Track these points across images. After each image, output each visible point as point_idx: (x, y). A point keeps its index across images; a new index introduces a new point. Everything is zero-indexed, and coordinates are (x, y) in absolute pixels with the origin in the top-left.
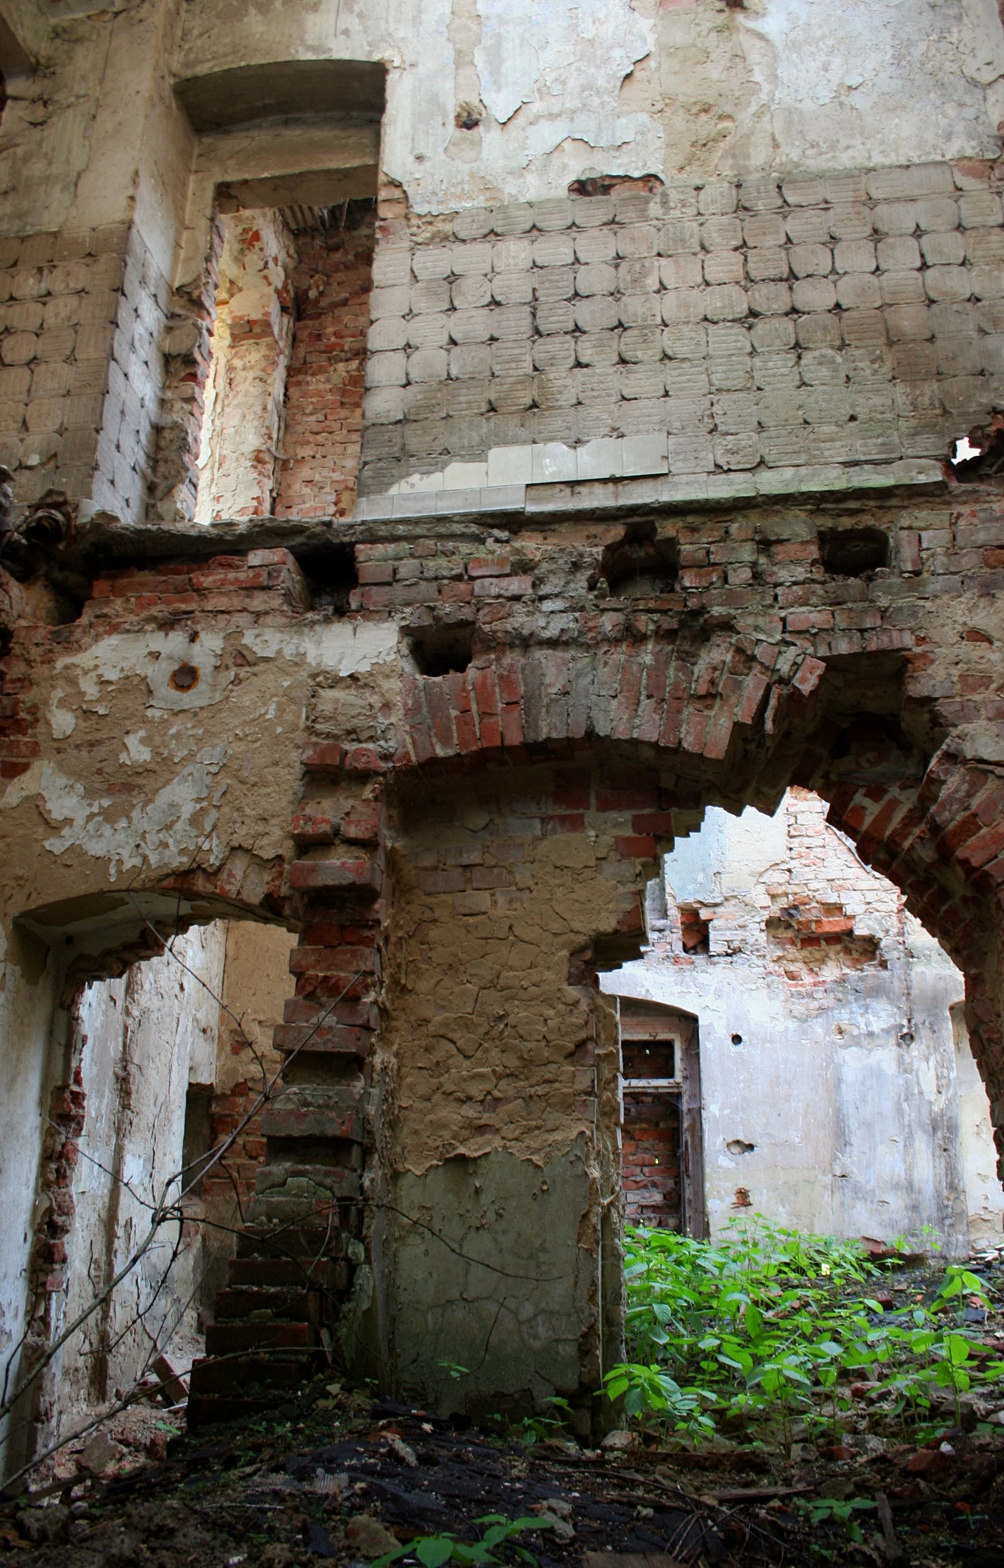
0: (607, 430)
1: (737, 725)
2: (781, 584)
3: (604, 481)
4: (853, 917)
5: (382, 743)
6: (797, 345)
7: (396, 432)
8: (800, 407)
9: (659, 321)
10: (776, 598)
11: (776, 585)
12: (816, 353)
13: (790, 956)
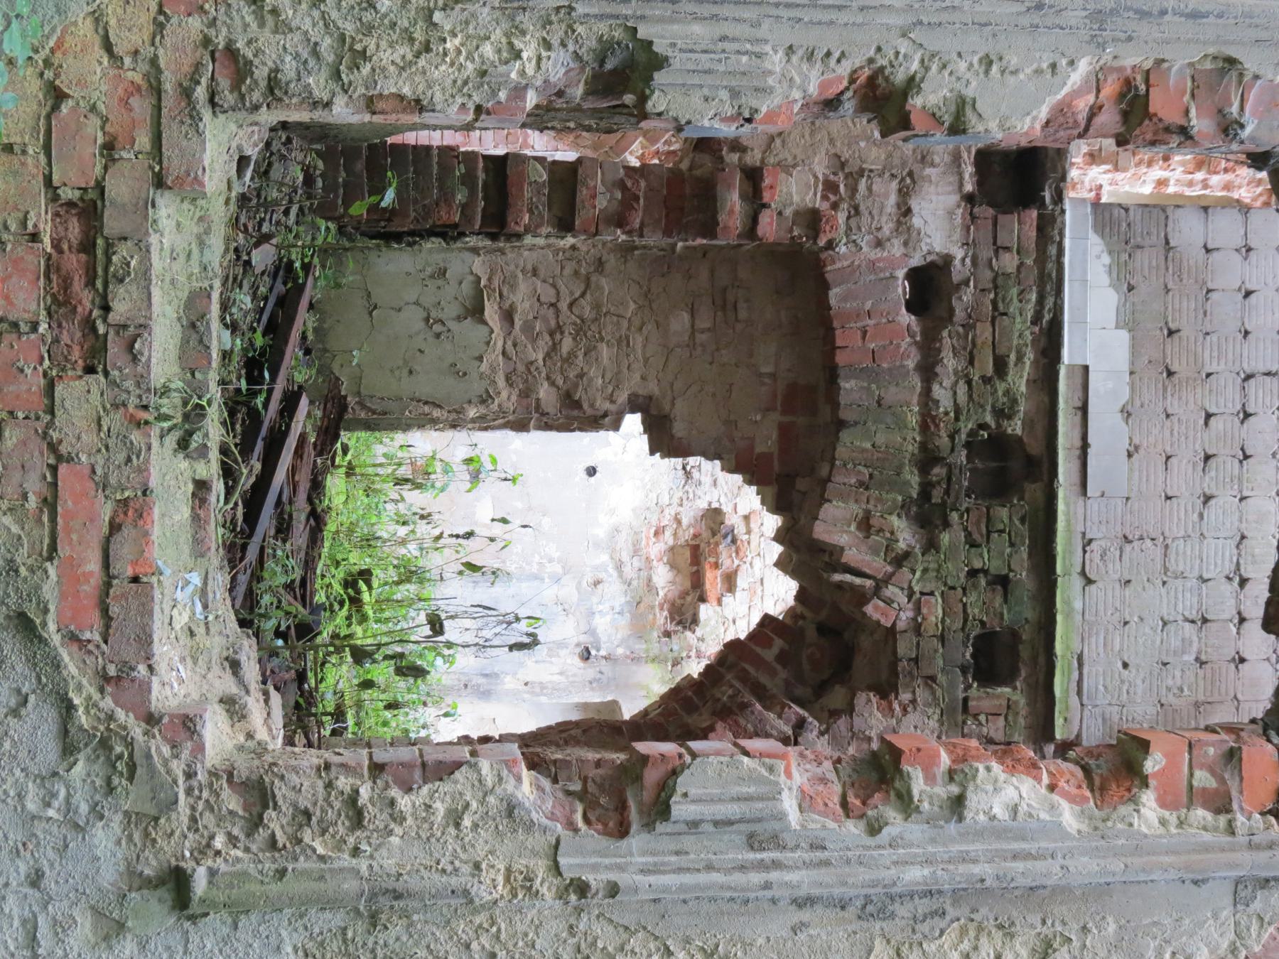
0: (1136, 441)
1: (842, 549)
2: (965, 594)
4: (719, 602)
5: (844, 240)
6: (1205, 621)
7: (1156, 239)
8: (1141, 619)
9: (1245, 493)
10: (953, 588)
11: (964, 589)
12: (1195, 639)
13: (680, 532)
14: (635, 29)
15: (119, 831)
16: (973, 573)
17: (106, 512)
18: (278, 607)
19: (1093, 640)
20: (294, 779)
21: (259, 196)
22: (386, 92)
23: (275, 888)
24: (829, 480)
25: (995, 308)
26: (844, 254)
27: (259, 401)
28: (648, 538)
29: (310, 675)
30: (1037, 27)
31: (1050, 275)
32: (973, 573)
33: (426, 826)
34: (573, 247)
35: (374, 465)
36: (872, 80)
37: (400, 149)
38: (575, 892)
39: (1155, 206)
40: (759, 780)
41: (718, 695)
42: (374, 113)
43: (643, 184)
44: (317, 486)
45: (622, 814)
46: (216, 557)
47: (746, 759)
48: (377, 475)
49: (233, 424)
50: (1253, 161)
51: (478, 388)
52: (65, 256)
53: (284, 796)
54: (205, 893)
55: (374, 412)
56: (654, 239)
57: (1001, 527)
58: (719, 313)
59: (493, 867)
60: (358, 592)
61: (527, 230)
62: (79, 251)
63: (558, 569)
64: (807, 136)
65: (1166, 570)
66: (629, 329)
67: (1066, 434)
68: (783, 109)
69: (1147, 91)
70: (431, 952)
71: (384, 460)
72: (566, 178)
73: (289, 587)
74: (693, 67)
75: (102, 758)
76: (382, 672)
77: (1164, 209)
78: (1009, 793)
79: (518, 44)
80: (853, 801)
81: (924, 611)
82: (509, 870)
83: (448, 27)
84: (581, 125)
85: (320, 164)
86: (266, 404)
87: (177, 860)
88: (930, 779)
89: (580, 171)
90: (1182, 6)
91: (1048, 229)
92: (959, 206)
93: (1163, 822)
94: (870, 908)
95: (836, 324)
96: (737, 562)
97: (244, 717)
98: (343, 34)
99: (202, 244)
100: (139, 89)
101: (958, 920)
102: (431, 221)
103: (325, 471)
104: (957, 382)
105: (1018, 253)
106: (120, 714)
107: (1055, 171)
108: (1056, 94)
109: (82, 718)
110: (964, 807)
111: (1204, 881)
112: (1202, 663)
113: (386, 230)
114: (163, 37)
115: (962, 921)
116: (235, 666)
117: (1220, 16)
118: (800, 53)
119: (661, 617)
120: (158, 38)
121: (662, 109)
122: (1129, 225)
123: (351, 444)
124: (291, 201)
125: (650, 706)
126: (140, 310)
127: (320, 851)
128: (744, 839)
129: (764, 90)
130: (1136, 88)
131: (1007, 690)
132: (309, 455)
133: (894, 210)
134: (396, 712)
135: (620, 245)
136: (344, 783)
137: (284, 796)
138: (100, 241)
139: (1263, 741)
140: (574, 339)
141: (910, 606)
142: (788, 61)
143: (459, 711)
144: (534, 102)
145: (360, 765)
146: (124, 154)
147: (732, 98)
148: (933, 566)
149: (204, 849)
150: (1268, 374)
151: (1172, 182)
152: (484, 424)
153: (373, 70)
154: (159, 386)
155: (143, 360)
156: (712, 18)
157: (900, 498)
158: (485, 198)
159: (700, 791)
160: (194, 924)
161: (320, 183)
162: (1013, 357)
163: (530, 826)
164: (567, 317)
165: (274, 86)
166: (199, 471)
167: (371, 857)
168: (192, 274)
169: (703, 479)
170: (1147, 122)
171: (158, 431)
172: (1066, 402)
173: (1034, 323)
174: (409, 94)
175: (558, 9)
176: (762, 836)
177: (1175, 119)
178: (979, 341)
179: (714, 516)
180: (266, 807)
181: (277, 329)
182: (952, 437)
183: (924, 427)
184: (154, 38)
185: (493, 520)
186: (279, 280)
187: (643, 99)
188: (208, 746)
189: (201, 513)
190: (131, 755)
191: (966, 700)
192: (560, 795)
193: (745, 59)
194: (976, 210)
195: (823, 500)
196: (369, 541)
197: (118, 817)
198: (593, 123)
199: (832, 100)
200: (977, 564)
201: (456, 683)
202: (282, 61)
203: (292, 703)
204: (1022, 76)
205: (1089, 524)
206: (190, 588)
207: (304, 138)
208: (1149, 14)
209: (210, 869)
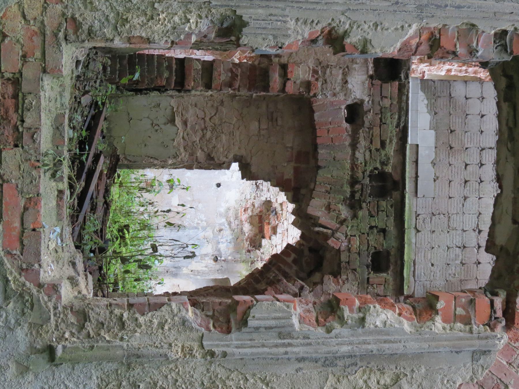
0: (437, 175)
1: (319, 218)
2: (368, 236)
3: (417, 173)
4: (270, 239)
5: (321, 93)
6: (464, 247)
8: (439, 246)
9: (481, 196)
10: (364, 234)
11: (368, 234)
12: (460, 254)
13: (254, 210)
14: (235, 11)
15: (27, 331)
16: (371, 228)
17: (22, 204)
18: (91, 240)
19: (420, 255)
20: (98, 310)
21: (84, 75)
22: (136, 35)
23: (89, 353)
24: (314, 190)
25: (381, 121)
26: (321, 99)
27: (84, 158)
28: (241, 212)
29: (104, 267)
30: (396, 11)
31: (403, 108)
32: (371, 228)
33: (150, 329)
34: (211, 95)
35: (131, 183)
36: (330, 32)
37: (141, 56)
38: (209, 355)
39: (445, 80)
40: (283, 311)
41: (269, 276)
42: (131, 44)
43: (240, 70)
44: (107, 191)
45: (228, 325)
46: (66, 221)
47: (278, 303)
48: (132, 186)
49: (73, 167)
50: (482, 65)
51: (173, 152)
52: (6, 100)
53: (93, 317)
54: (61, 355)
55: (130, 161)
56: (244, 92)
57: (383, 209)
58: (270, 123)
59: (177, 345)
60: (124, 234)
61: (193, 89)
62: (12, 98)
63: (205, 224)
64: (306, 51)
65: (449, 227)
66: (233, 129)
67: (409, 172)
68: (295, 43)
69: (440, 37)
70: (152, 379)
71: (134, 180)
72: (209, 68)
73: (96, 232)
74: (258, 26)
75: (20, 302)
76: (133, 267)
77: (449, 82)
78: (383, 317)
79: (189, 16)
80: (321, 319)
81: (352, 242)
82: (183, 347)
83: (160, 10)
84: (214, 48)
85: (109, 61)
86: (87, 159)
87: (50, 342)
88: (351, 311)
89: (214, 65)
90: (454, 3)
91: (403, 90)
92: (367, 80)
93: (444, 328)
94: (327, 362)
95: (317, 127)
96: (277, 222)
97: (77, 285)
98: (119, 12)
99: (61, 96)
100: (36, 33)
101: (362, 367)
102: (154, 85)
103: (111, 185)
104: (366, 151)
105: (391, 99)
106: (28, 284)
107: (405, 66)
108: (403, 38)
109: (12, 285)
110: (365, 322)
111: (460, 352)
112: (463, 264)
113: (137, 89)
114: (46, 13)
115: (364, 367)
116: (74, 264)
117: (469, 7)
118: (301, 21)
119: (246, 244)
120: (44, 13)
121: (246, 43)
122: (435, 88)
123: (121, 174)
124: (97, 78)
125: (242, 280)
126: (36, 122)
127: (108, 338)
128: (277, 334)
129: (287, 36)
130: (435, 36)
131: (385, 275)
132: (104, 179)
133: (341, 81)
134: (139, 282)
135: (230, 95)
136: (117, 311)
137: (93, 317)
138: (20, 94)
139: (484, 296)
140: (212, 132)
141: (346, 240)
142: (297, 24)
143: (164, 282)
144: (195, 40)
145: (124, 304)
146: (30, 60)
147: (274, 38)
148: (355, 224)
149: (61, 338)
150: (490, 148)
151: (453, 70)
152: (175, 166)
153: (130, 26)
154: (44, 152)
155: (38, 142)
156: (266, 7)
157: (342, 197)
158: (176, 75)
159: (260, 315)
160: (57, 368)
161: (109, 69)
162: (388, 141)
163: (191, 329)
164: (209, 124)
165: (90, 32)
166: (60, 186)
167: (128, 341)
168: (57, 108)
169: (264, 188)
170: (439, 49)
171: (43, 170)
172: (409, 159)
173: (397, 127)
174: (145, 36)
175: (205, 2)
176: (284, 333)
177: (451, 48)
178: (374, 134)
179: (268, 203)
180: (86, 321)
181: (91, 128)
182: (363, 173)
183: (352, 169)
184: (42, 13)
185: (178, 205)
186: (92, 109)
187: (238, 39)
188: (63, 296)
189: (61, 203)
190: (32, 300)
191: (368, 279)
192: (204, 316)
193: (279, 23)
194: (374, 82)
195: (311, 198)
196: (128, 214)
197: (26, 325)
198: (219, 47)
199: (314, 40)
200: (373, 224)
201: (163, 270)
202: (94, 23)
203: (97, 279)
204: (390, 31)
205: (418, 208)
206: (56, 234)
207: (103, 52)
208: (440, 6)
209: (63, 345)
